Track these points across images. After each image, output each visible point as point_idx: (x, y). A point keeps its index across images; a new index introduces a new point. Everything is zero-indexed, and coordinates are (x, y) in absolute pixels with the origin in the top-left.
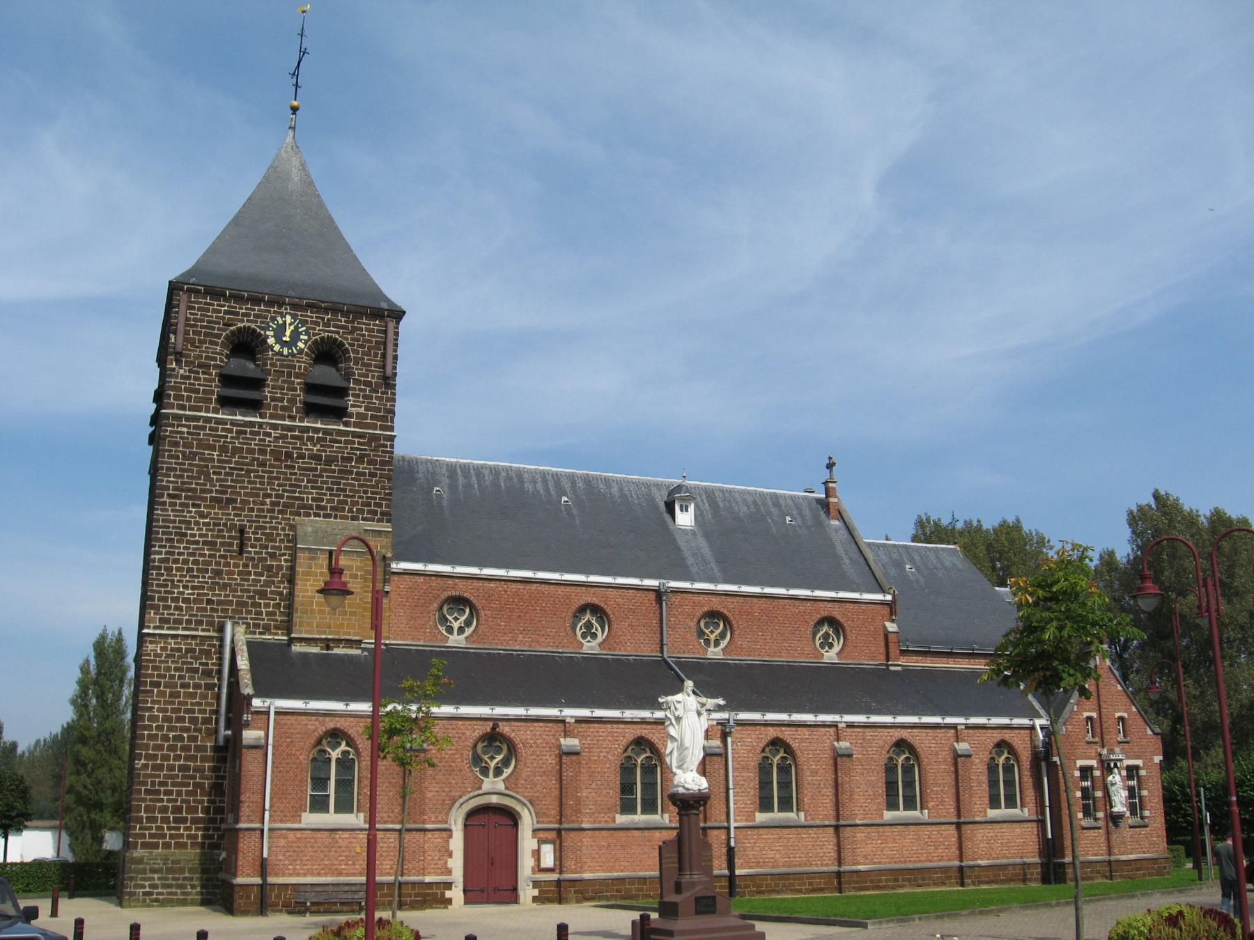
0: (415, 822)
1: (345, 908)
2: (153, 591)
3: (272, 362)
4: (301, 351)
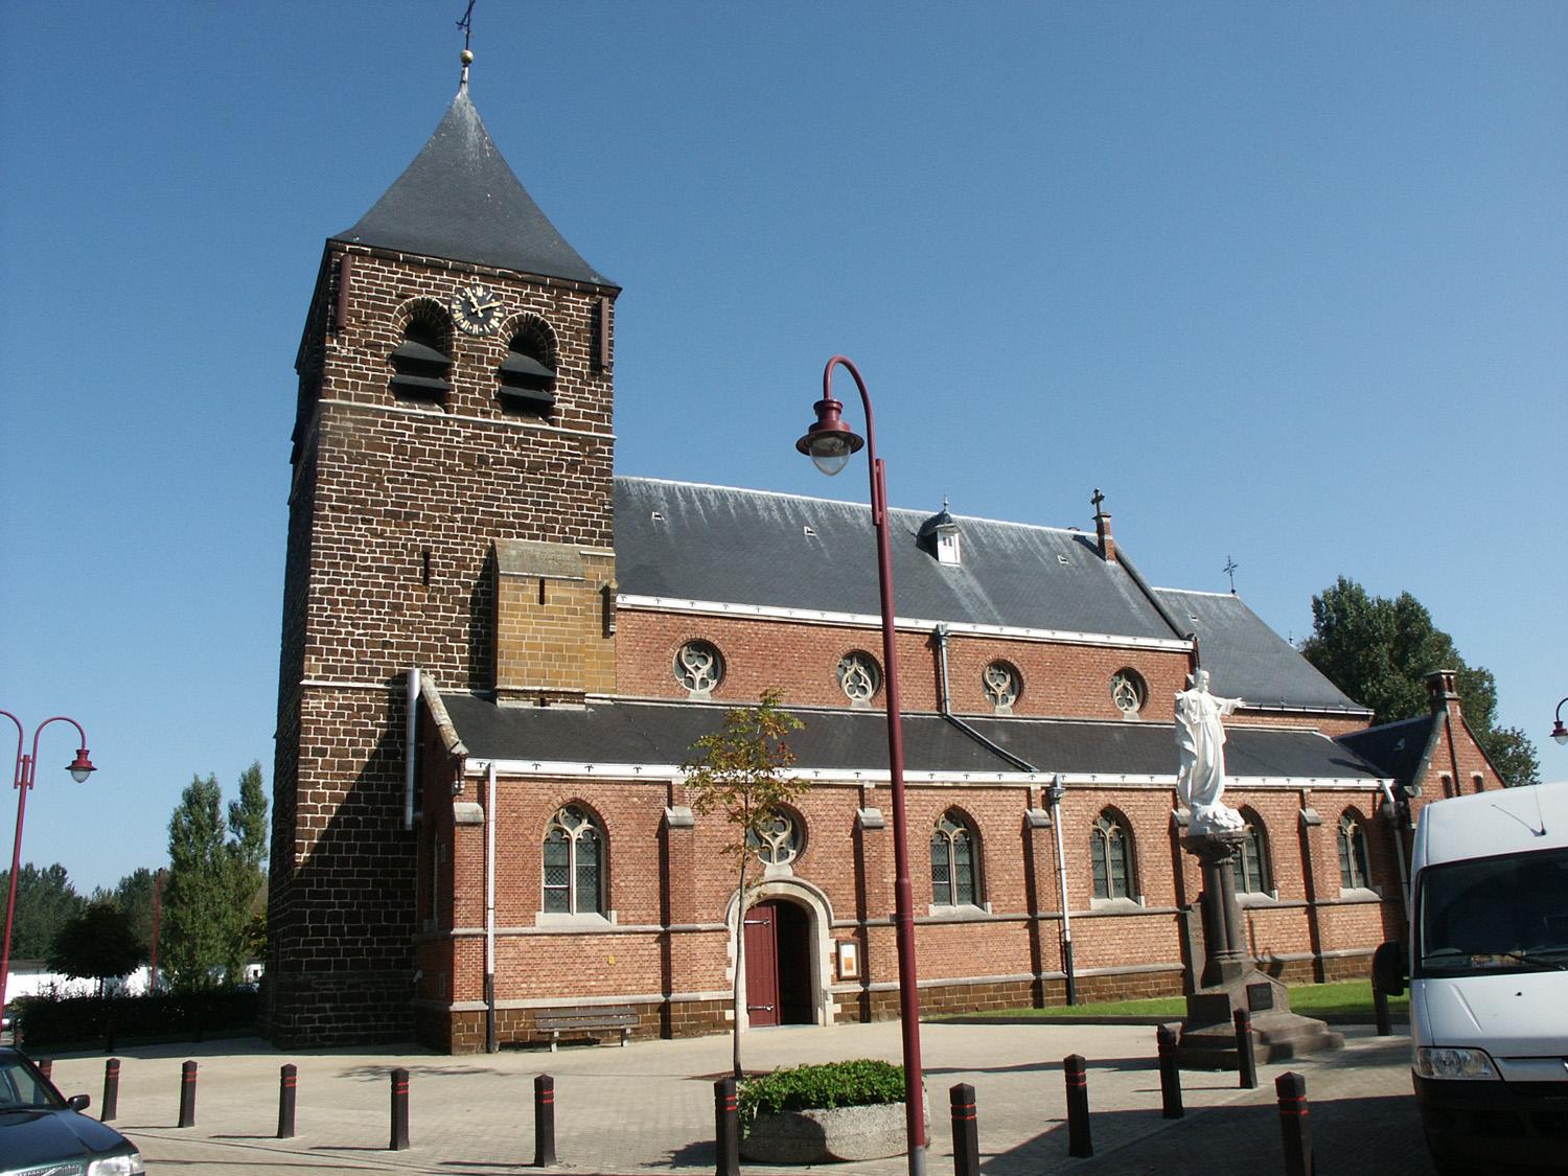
0: (684, 922)
1: (328, 1043)
2: (312, 631)
4: (494, 332)
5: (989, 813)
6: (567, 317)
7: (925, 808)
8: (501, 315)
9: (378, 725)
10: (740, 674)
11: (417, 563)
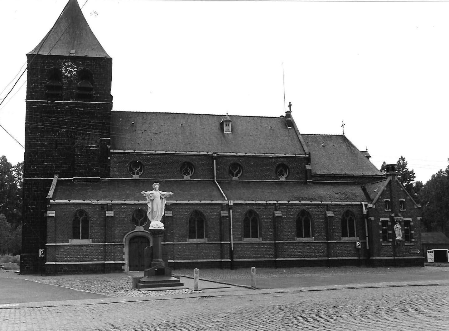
5: (208, 212)
10: (148, 170)
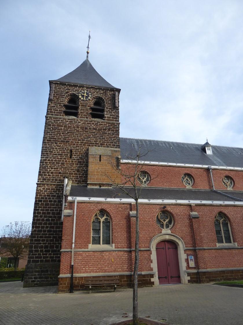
3: (82, 106)
4: (89, 100)
5: (232, 214)
6: (106, 98)
7: (212, 212)
8: (91, 96)
9: (56, 194)
11: (69, 153)
